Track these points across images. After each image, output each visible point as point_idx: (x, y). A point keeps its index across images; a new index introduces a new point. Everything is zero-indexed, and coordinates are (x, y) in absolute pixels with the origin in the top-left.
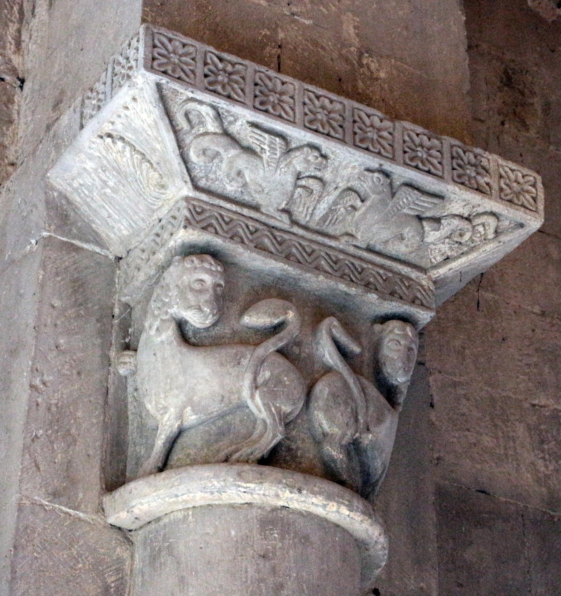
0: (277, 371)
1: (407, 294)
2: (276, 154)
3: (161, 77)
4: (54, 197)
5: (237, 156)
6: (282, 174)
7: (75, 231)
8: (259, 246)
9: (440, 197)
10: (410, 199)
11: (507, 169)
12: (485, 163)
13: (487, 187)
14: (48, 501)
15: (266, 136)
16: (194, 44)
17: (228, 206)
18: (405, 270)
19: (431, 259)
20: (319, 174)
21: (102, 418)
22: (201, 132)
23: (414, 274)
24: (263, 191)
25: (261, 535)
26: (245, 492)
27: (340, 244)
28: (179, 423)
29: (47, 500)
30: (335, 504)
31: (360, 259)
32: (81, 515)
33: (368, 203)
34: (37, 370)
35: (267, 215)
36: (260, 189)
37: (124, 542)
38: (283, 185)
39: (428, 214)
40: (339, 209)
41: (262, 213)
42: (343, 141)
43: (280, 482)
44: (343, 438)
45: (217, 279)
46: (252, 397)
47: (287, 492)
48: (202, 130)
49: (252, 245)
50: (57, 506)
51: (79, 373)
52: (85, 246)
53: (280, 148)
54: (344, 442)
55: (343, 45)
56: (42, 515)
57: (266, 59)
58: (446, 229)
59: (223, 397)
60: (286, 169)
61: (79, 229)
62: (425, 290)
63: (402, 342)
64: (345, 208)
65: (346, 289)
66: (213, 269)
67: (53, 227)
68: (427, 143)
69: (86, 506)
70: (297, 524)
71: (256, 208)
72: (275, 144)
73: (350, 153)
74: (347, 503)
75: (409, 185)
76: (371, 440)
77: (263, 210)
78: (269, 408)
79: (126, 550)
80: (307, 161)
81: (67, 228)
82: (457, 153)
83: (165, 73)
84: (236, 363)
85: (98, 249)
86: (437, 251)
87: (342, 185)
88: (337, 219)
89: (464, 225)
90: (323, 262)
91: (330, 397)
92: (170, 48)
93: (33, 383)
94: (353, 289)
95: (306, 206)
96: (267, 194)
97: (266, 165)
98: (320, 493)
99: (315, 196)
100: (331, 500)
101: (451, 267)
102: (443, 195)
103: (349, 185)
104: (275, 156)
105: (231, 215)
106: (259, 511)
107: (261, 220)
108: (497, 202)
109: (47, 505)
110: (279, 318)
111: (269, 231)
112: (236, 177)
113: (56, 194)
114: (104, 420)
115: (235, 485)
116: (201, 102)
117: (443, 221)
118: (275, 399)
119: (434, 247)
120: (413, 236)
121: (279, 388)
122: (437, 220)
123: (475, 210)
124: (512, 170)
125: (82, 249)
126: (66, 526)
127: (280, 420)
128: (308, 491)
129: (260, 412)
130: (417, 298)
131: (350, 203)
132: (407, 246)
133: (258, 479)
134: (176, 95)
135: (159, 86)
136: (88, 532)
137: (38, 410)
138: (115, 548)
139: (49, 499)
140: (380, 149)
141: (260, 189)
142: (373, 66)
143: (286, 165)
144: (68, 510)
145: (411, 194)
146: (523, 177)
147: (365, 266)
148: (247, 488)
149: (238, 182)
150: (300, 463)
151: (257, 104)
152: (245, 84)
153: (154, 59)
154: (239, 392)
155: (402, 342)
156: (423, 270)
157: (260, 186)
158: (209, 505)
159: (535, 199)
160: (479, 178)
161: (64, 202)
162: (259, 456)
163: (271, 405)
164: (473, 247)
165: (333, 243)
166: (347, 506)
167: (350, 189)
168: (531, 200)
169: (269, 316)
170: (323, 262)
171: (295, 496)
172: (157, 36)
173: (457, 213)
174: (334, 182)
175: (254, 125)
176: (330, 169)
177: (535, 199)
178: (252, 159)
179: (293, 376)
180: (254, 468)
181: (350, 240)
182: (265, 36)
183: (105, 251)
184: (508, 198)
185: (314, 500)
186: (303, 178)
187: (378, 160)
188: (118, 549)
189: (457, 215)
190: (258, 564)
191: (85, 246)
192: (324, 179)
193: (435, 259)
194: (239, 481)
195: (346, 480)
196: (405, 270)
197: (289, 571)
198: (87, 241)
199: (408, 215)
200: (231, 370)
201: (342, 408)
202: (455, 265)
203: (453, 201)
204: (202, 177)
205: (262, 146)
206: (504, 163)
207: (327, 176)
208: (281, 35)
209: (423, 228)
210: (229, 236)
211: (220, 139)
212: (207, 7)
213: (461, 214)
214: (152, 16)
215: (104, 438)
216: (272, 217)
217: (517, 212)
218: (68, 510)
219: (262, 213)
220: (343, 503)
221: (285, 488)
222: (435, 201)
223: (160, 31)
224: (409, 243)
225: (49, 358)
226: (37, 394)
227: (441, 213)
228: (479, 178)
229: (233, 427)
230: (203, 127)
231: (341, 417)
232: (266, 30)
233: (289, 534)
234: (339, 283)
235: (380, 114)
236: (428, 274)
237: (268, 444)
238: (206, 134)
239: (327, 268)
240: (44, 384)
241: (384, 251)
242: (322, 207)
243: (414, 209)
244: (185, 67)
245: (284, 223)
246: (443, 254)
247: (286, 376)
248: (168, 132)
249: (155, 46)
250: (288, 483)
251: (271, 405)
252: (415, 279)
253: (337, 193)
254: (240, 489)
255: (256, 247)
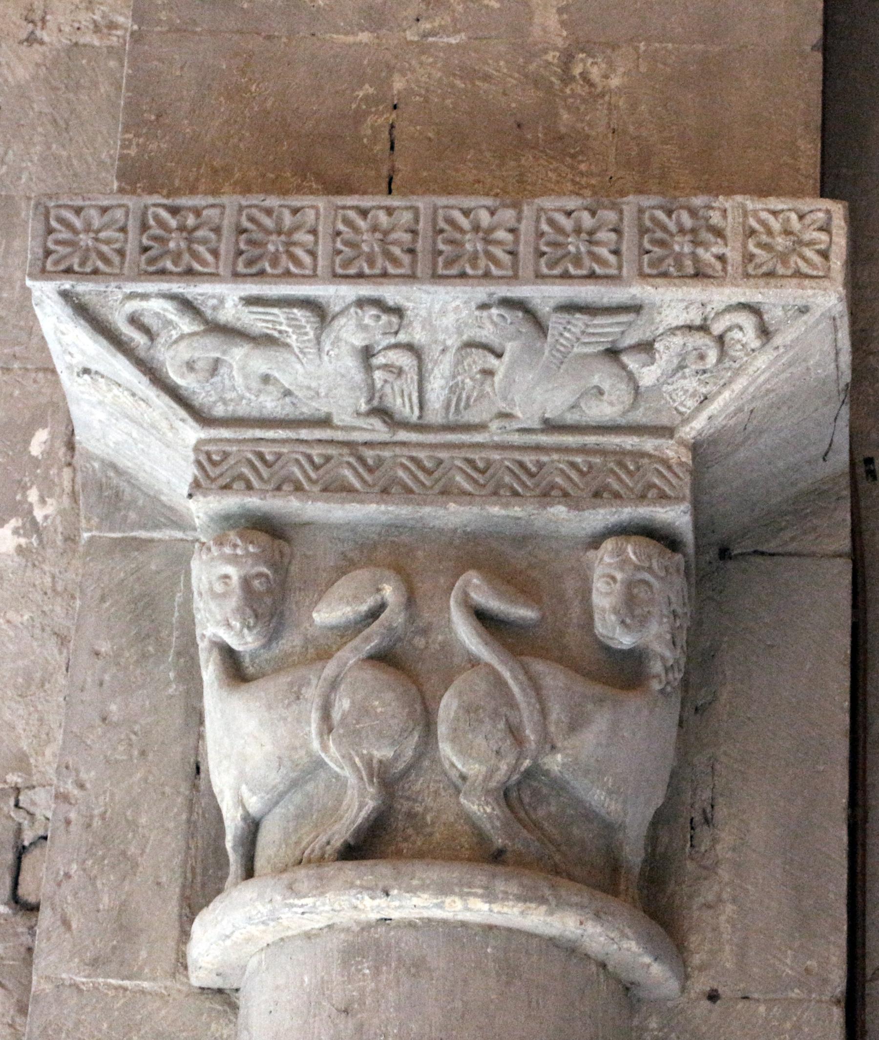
0: (359, 697)
1: (631, 485)
2: (306, 334)
3: (58, 283)
4: (94, 470)
5: (246, 355)
6: (334, 361)
7: (133, 515)
8: (332, 487)
9: (635, 308)
10: (573, 329)
11: (764, 215)
12: (716, 218)
13: (718, 266)
14: (85, 977)
15: (275, 311)
16: (122, 202)
17: (271, 434)
18: (629, 442)
19: (676, 409)
20: (402, 337)
21: (184, 816)
22: (175, 337)
23: (649, 444)
24: (318, 394)
25: (343, 976)
26: (303, 913)
27: (495, 433)
28: (240, 812)
29: (82, 974)
30: (457, 899)
31: (538, 448)
32: (146, 985)
33: (506, 358)
34: (67, 767)
35: (344, 428)
36: (312, 393)
37: (225, 1011)
38: (343, 376)
39: (630, 340)
40: (463, 382)
41: (337, 428)
42: (412, 277)
43: (352, 886)
44: (491, 777)
45: (248, 568)
46: (325, 747)
47: (366, 898)
48: (175, 334)
49: (316, 489)
50: (101, 980)
51: (143, 753)
52: (156, 535)
53: (308, 322)
54: (493, 784)
55: (531, 56)
56: (73, 1001)
57: (365, 140)
58: (665, 357)
59: (280, 758)
60: (336, 350)
61: (141, 511)
62: (669, 468)
63: (619, 576)
64: (472, 379)
65: (503, 512)
66: (239, 552)
67: (95, 520)
68: (587, 221)
69: (153, 970)
70: (403, 945)
71: (325, 422)
72: (296, 319)
73: (429, 293)
74: (480, 891)
75: (570, 308)
76: (563, 764)
77: (336, 421)
78: (351, 759)
79: (227, 1025)
80: (365, 328)
81: (118, 516)
82: (653, 219)
83: (69, 271)
84: (292, 698)
85: (179, 535)
86: (681, 393)
87: (453, 342)
88: (468, 398)
89: (699, 340)
90: (459, 478)
91: (461, 712)
92: (78, 223)
93: (62, 790)
94: (517, 508)
95: (406, 393)
96: (327, 395)
97: (301, 356)
98: (423, 887)
99: (412, 375)
100: (446, 895)
101: (710, 414)
102: (638, 302)
103: (465, 337)
104: (306, 338)
105: (277, 449)
106: (342, 936)
107: (335, 438)
108: (737, 286)
109: (83, 983)
110: (365, 601)
111: (351, 454)
112: (262, 386)
113: (96, 465)
114: (189, 821)
115: (286, 905)
116: (145, 296)
117: (657, 345)
118: (359, 744)
119: (670, 388)
120: (613, 386)
121: (366, 723)
122: (646, 347)
123: (709, 309)
124: (775, 213)
125: (152, 541)
126: (118, 1009)
127: (371, 776)
128: (400, 889)
129: (342, 768)
130: (651, 486)
131: (475, 369)
132: (611, 404)
133: (317, 888)
134: (105, 297)
135: (65, 295)
136: (159, 1009)
137: (68, 832)
138: (208, 1025)
139: (87, 972)
140: (487, 266)
141: (312, 393)
142: (595, 73)
143: (333, 344)
144: (121, 982)
145: (573, 321)
146: (801, 217)
147: (544, 458)
148: (302, 906)
149: (270, 393)
150: (431, 834)
151: (241, 268)
152: (219, 240)
153: (48, 253)
154: (306, 744)
155: (619, 576)
156: (667, 431)
157: (309, 388)
158: (282, 939)
159: (825, 255)
160: (700, 251)
161: (111, 474)
162: (338, 843)
163: (353, 753)
164: (738, 369)
165: (478, 438)
166: (481, 896)
167: (470, 344)
168: (817, 259)
169: (348, 603)
170: (459, 478)
171: (382, 901)
172: (53, 213)
173: (680, 322)
174: (436, 342)
175: (251, 301)
176: (417, 326)
177: (825, 255)
178: (271, 352)
179: (389, 696)
180: (311, 872)
181: (505, 423)
182: (366, 98)
183: (188, 533)
184: (764, 269)
185: (415, 901)
186: (380, 351)
187: (482, 288)
188: (213, 1026)
189: (678, 328)
190: (335, 1025)
191: (156, 535)
192: (416, 342)
193: (685, 406)
194: (289, 898)
195: (505, 846)
196: (629, 442)
197: (386, 1026)
198: (157, 527)
199: (586, 356)
200: (285, 713)
201: (487, 726)
202: (714, 408)
203: (661, 307)
204: (215, 403)
205: (278, 327)
206: (759, 206)
207: (418, 337)
208: (398, 84)
209: (624, 367)
210: (272, 486)
211: (201, 341)
212: (247, 90)
213: (688, 322)
214: (138, 145)
215: (189, 848)
216: (354, 428)
217: (784, 290)
218: (121, 982)
219: (337, 428)
220: (469, 894)
221: (361, 893)
222: (624, 318)
223: (60, 202)
224: (613, 398)
225: (89, 742)
226: (67, 806)
227: (652, 332)
228: (700, 251)
229: (315, 800)
230: (175, 328)
231: (484, 743)
232: (367, 86)
233: (388, 964)
234: (487, 507)
235: (489, 202)
236: (677, 436)
237: (353, 822)
238: (182, 337)
239: (467, 486)
240: (82, 786)
241: (584, 420)
242: (436, 386)
243: (589, 343)
244: (105, 248)
245: (378, 431)
246: (693, 395)
247: (377, 698)
248: (115, 356)
249: (50, 231)
250: (364, 883)
251: (353, 753)
252: (652, 452)
253: (449, 358)
254: (295, 909)
255: (325, 490)
